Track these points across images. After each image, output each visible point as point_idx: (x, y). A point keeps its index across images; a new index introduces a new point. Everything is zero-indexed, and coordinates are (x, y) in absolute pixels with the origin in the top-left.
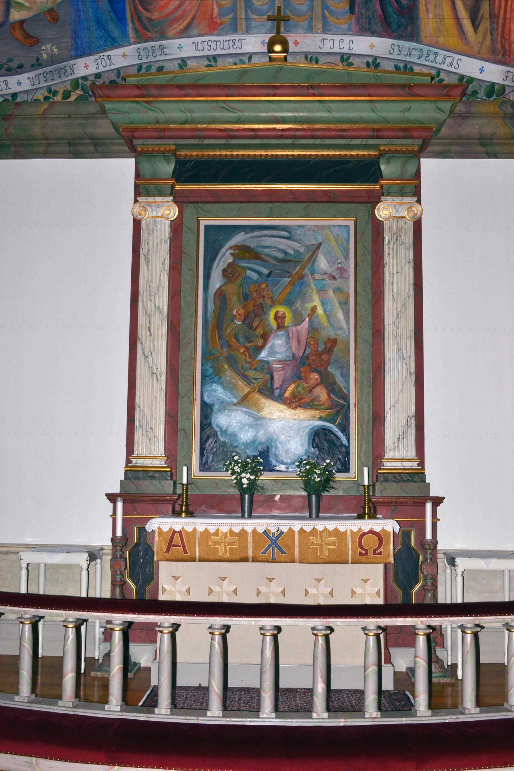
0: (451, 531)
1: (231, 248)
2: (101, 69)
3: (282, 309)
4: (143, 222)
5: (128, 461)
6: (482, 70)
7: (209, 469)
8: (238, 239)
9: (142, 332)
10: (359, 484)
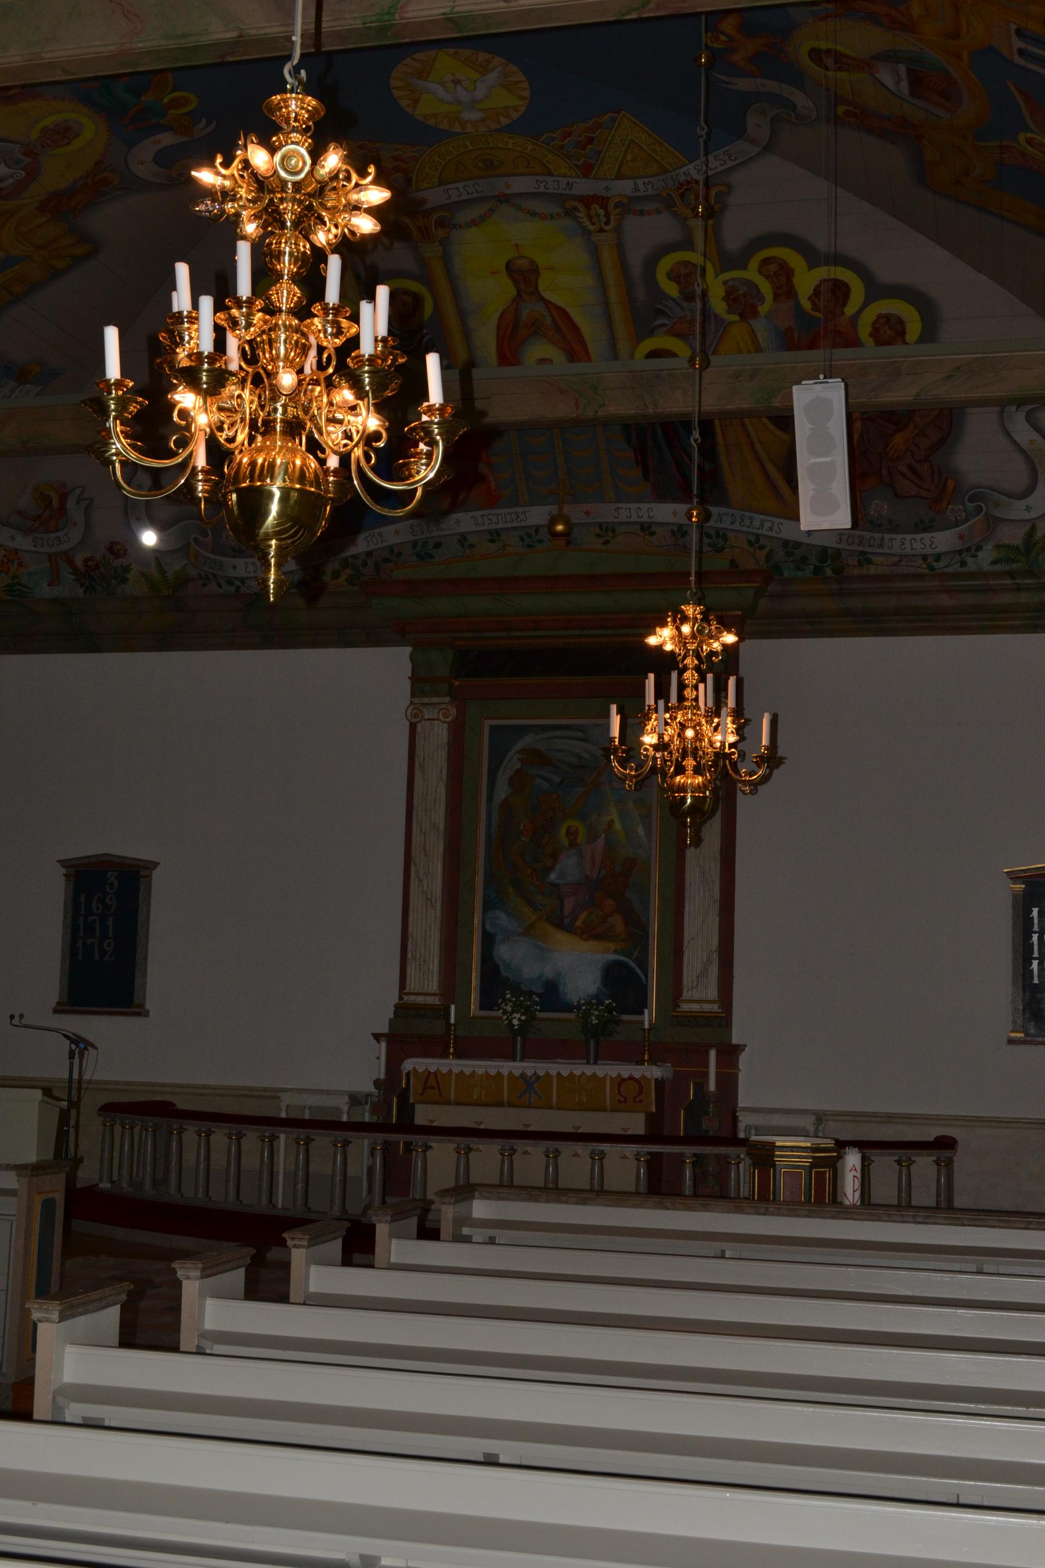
1: (518, 752)
2: (373, 547)
8: (527, 741)
9: (416, 851)
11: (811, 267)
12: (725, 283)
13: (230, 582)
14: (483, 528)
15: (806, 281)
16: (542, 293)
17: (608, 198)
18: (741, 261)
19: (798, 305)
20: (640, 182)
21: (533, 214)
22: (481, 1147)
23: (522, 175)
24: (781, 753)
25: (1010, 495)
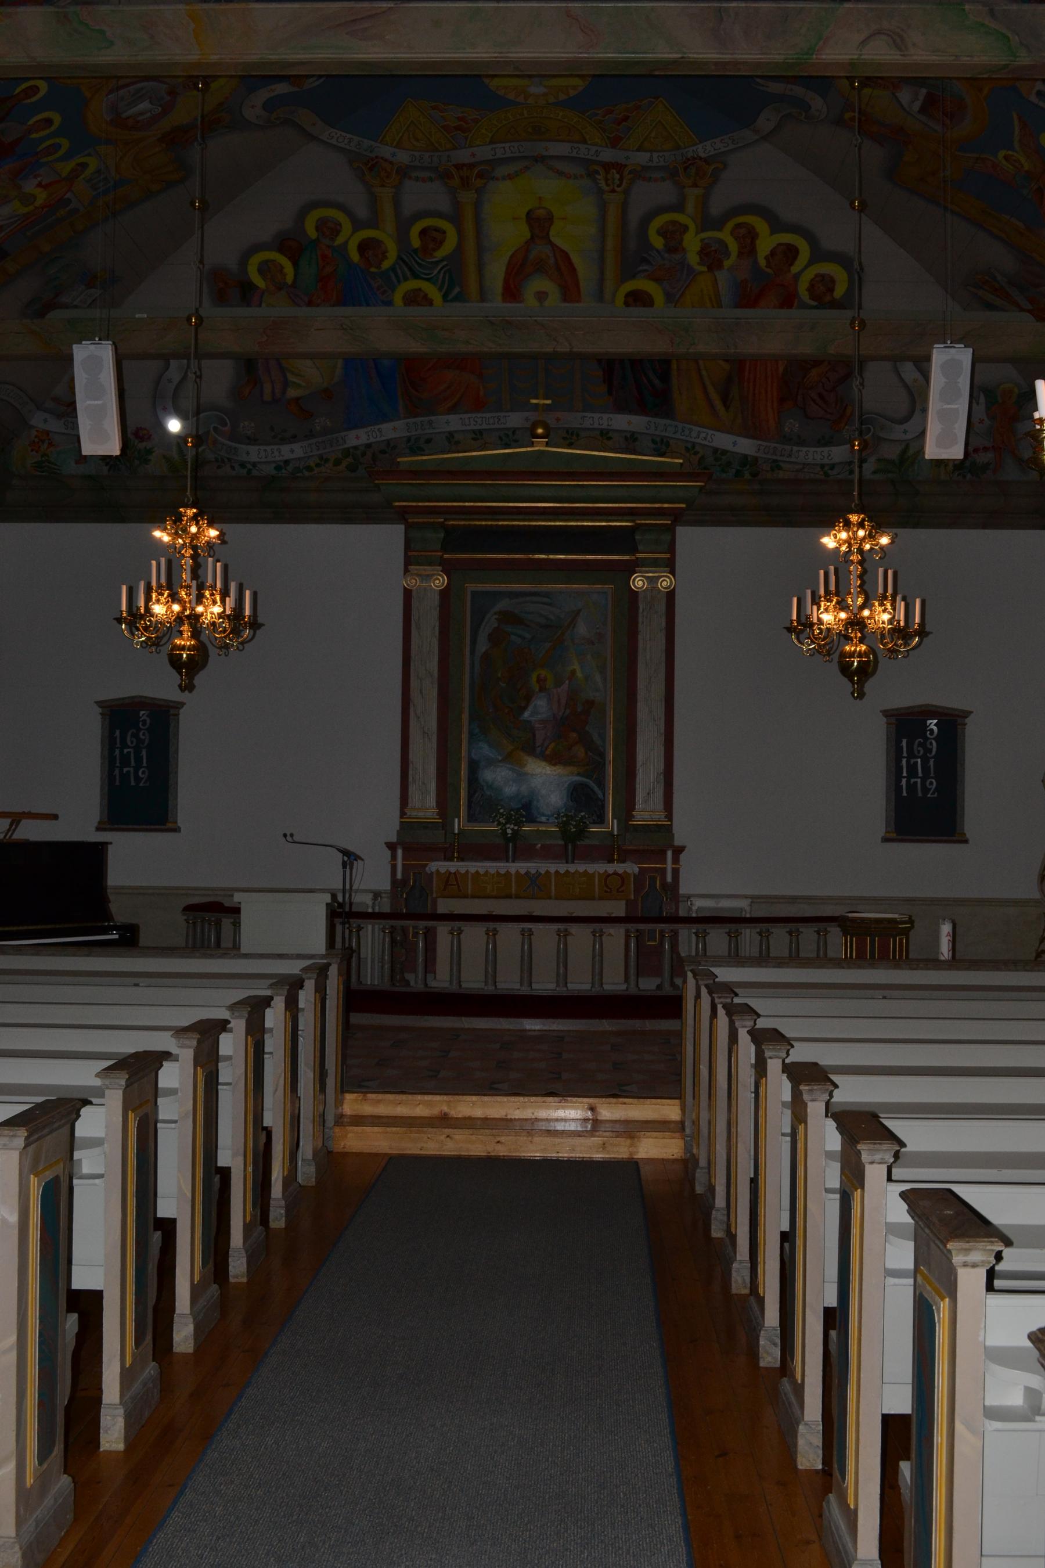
1: (495, 614)
2: (372, 440)
3: (543, 673)
4: (414, 593)
5: (403, 814)
6: (735, 444)
7: (476, 821)
9: (414, 694)
10: (611, 833)
11: (772, 233)
12: (702, 240)
13: (243, 465)
14: (468, 428)
15: (766, 243)
16: (552, 239)
17: (626, 166)
18: (718, 224)
19: (756, 262)
20: (655, 155)
21: (561, 174)
22: (612, 931)
23: (563, 141)
24: (927, 629)
25: (893, 421)
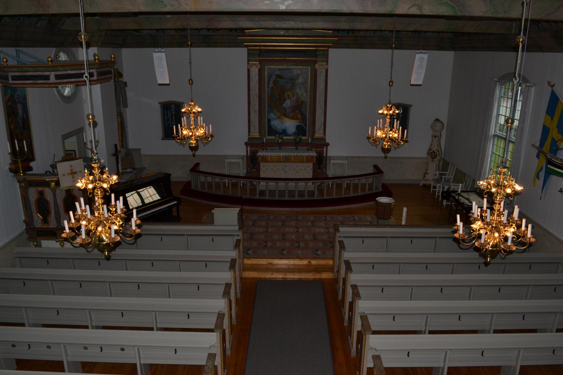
0: (332, 152)
3: (289, 93)
5: (249, 135)
9: (251, 100)
